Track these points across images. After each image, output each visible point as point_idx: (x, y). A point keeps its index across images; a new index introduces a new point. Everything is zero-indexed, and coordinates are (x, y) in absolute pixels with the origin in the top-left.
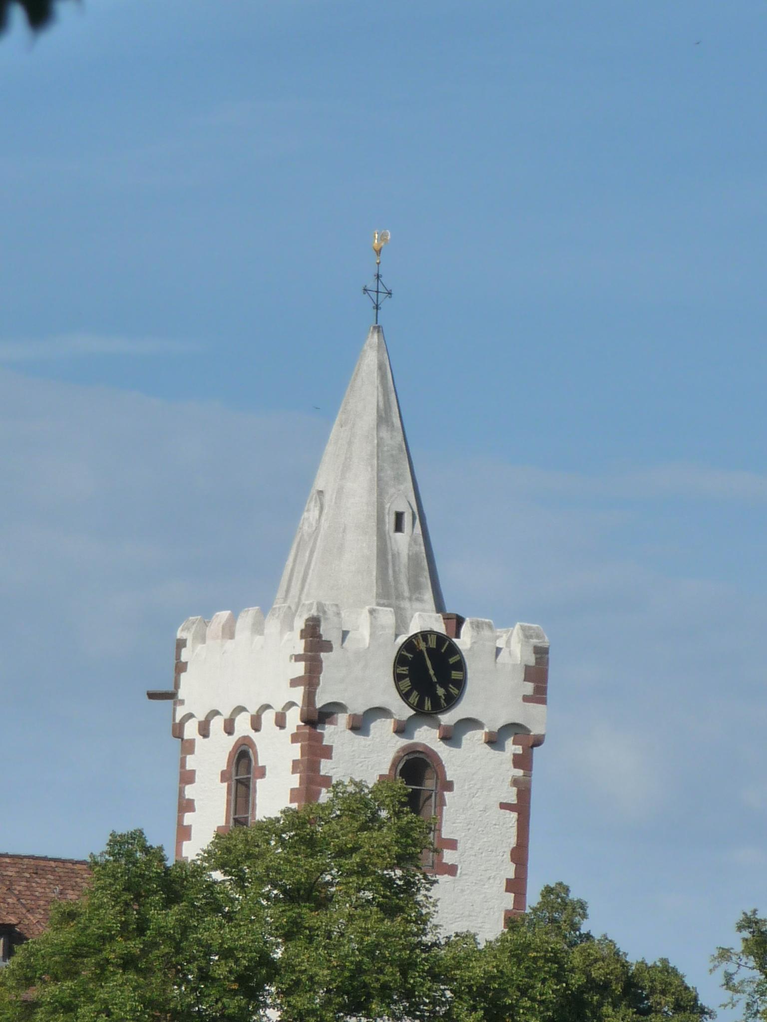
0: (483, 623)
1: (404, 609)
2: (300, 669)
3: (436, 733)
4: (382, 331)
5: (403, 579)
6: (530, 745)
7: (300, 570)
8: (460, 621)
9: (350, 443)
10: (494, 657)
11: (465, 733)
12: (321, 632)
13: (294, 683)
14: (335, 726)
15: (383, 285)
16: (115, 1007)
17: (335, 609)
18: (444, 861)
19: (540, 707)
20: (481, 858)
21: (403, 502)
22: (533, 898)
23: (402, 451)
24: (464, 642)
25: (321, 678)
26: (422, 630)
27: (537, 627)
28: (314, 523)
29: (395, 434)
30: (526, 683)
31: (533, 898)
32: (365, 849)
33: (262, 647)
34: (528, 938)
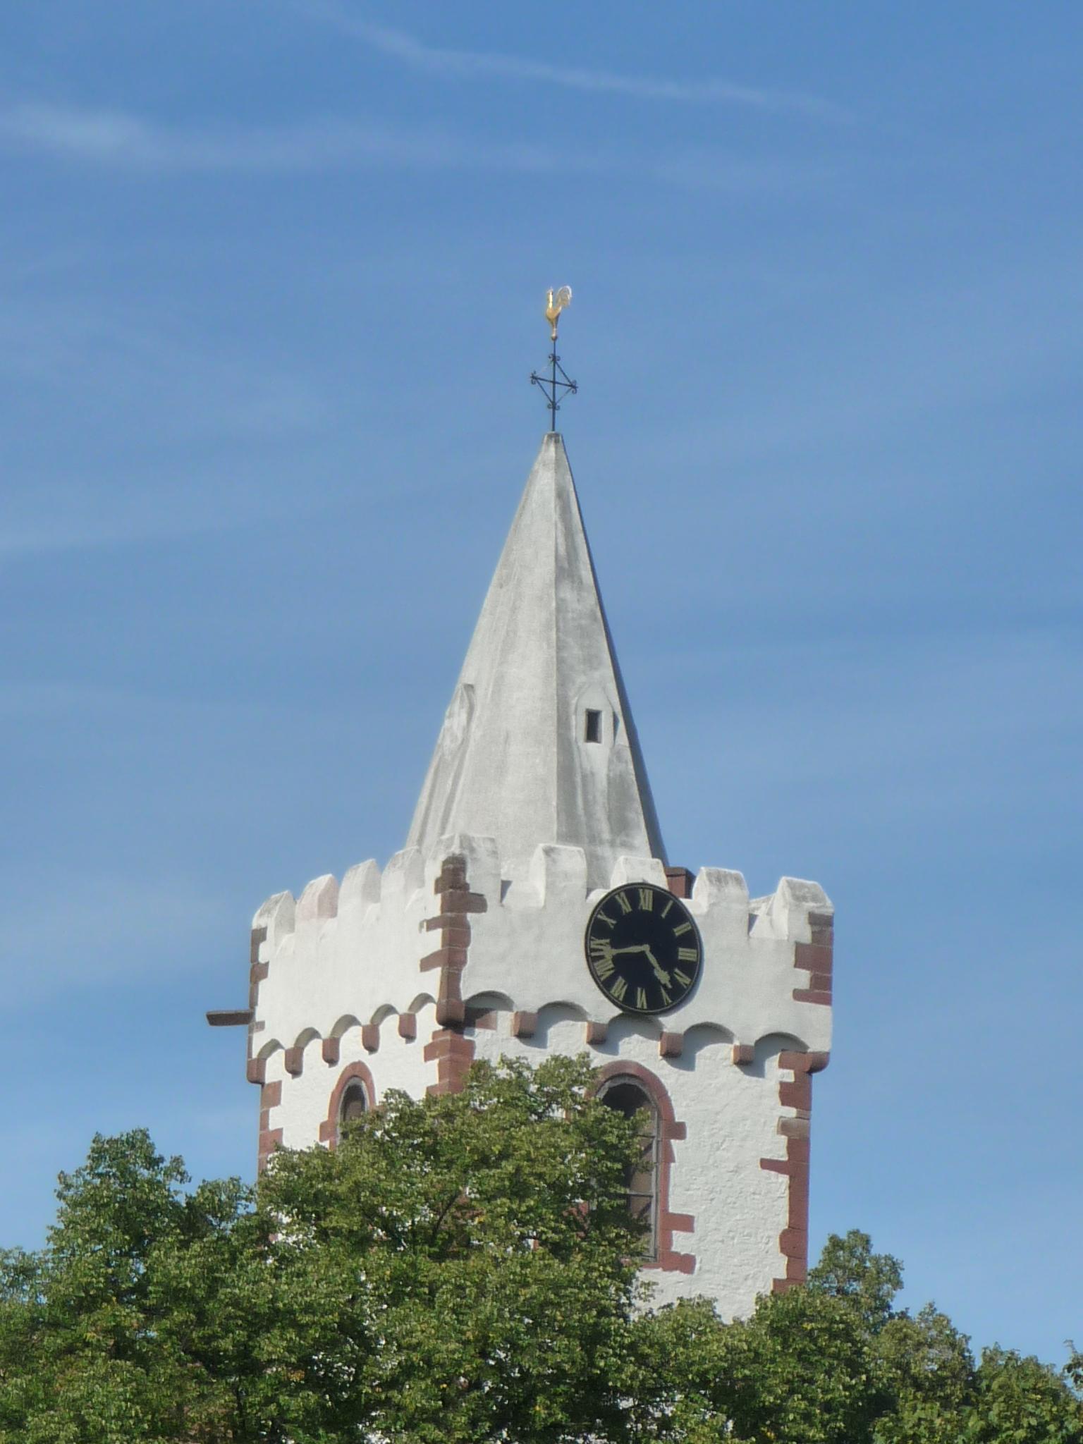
0: (726, 875)
1: (603, 858)
2: (434, 941)
3: (656, 1047)
4: (563, 441)
5: (600, 813)
6: (807, 1070)
7: (439, 805)
8: (690, 879)
9: (514, 609)
10: (746, 928)
11: (700, 1047)
12: (468, 880)
13: (426, 964)
14: (494, 1031)
15: (562, 371)
16: (92, 1411)
17: (489, 845)
18: (674, 1249)
19: (822, 1011)
20: (733, 1245)
21: (605, 700)
22: (814, 1258)
23: (595, 619)
24: (697, 904)
25: (469, 954)
26: (630, 882)
27: (815, 885)
28: (460, 735)
29: (585, 594)
30: (798, 970)
31: (814, 1258)
32: (523, 1152)
33: (378, 919)
34: (800, 1301)
